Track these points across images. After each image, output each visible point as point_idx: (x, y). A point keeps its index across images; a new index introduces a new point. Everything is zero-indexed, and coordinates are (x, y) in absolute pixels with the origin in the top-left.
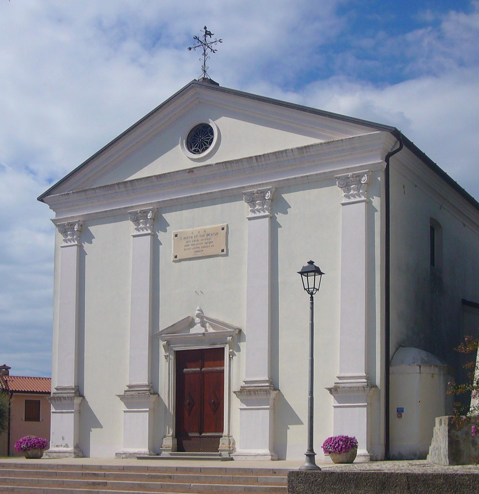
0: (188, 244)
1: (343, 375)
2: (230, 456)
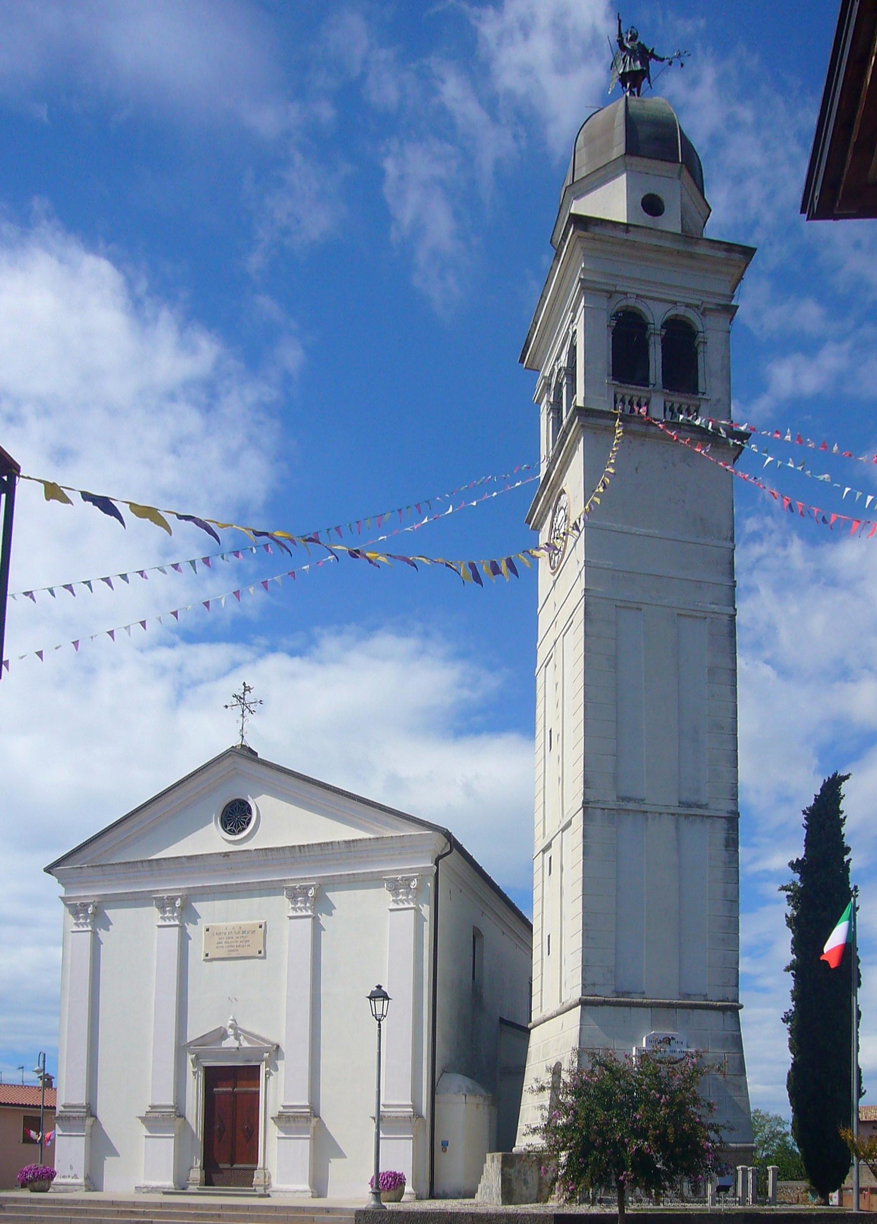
0: (220, 941)
2: (265, 1192)
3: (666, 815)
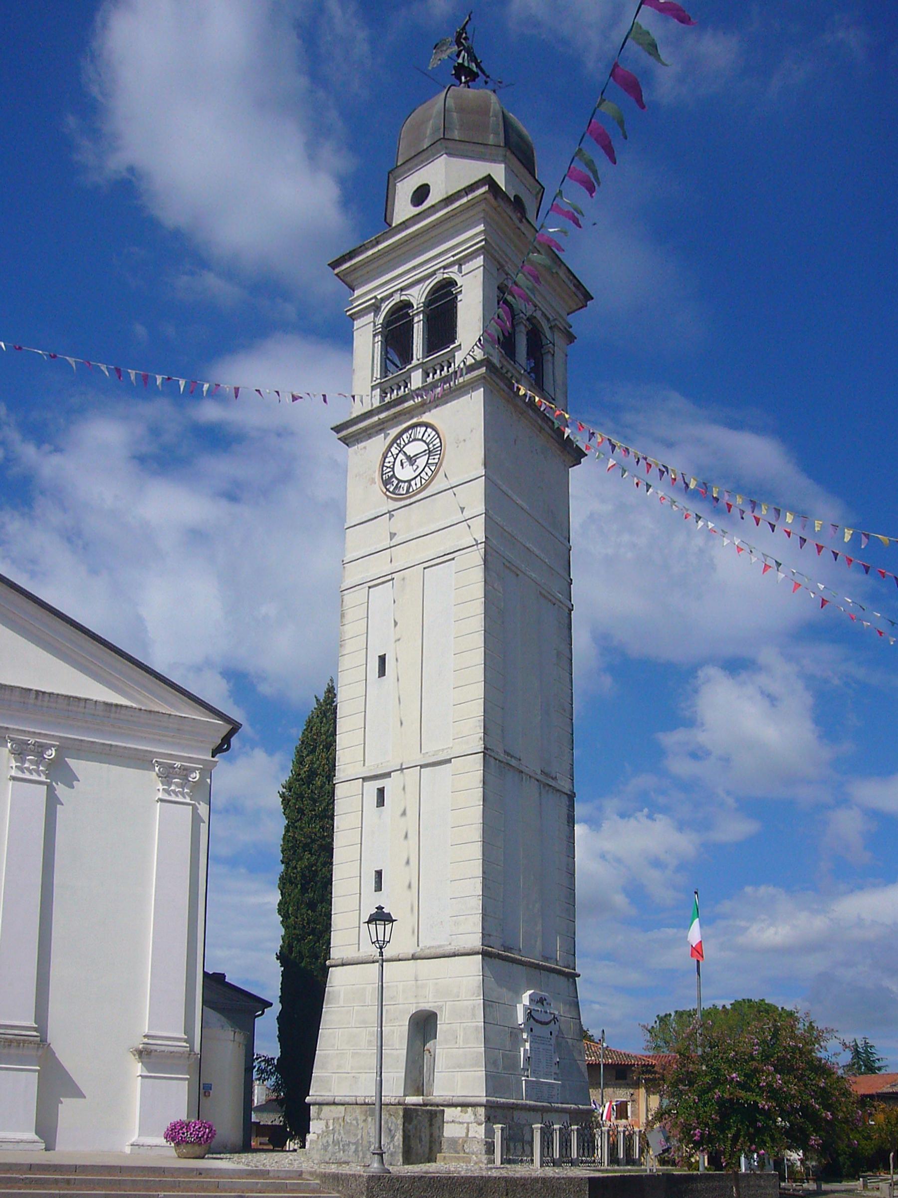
1: (153, 1033)
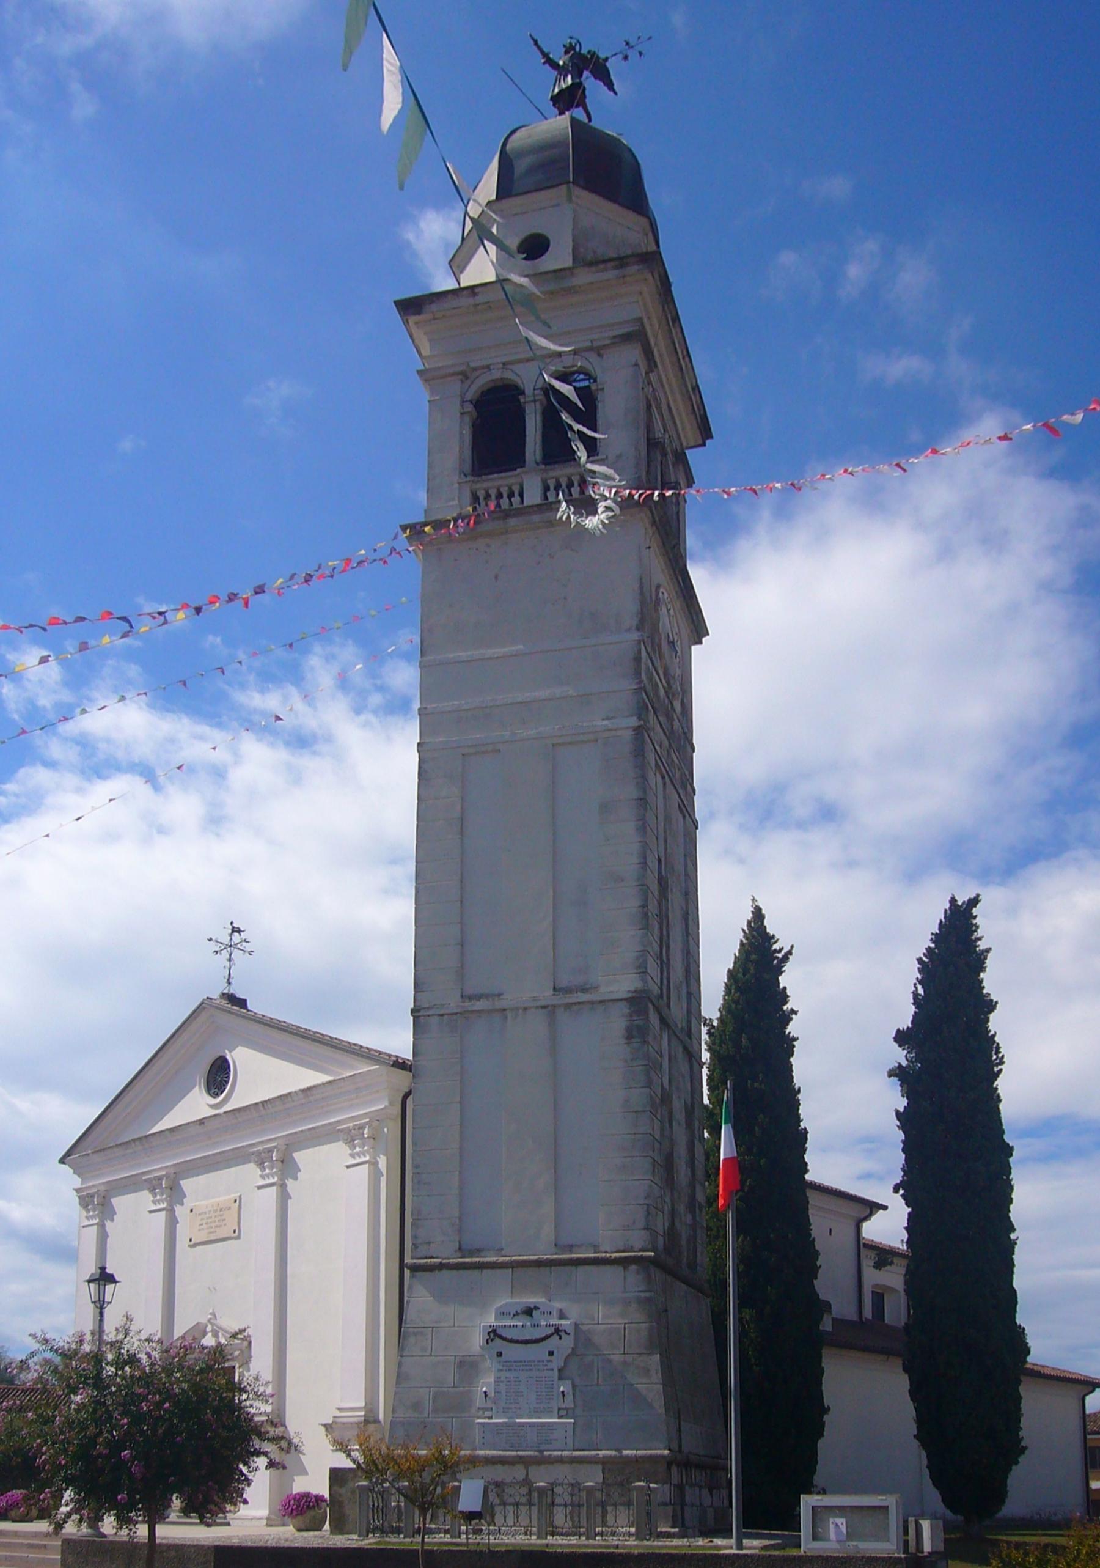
3: (533, 1010)
